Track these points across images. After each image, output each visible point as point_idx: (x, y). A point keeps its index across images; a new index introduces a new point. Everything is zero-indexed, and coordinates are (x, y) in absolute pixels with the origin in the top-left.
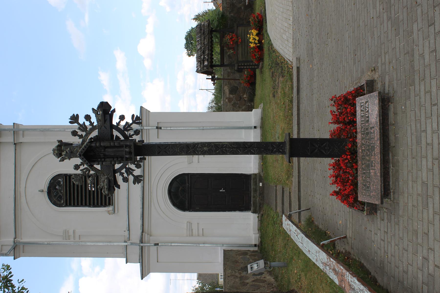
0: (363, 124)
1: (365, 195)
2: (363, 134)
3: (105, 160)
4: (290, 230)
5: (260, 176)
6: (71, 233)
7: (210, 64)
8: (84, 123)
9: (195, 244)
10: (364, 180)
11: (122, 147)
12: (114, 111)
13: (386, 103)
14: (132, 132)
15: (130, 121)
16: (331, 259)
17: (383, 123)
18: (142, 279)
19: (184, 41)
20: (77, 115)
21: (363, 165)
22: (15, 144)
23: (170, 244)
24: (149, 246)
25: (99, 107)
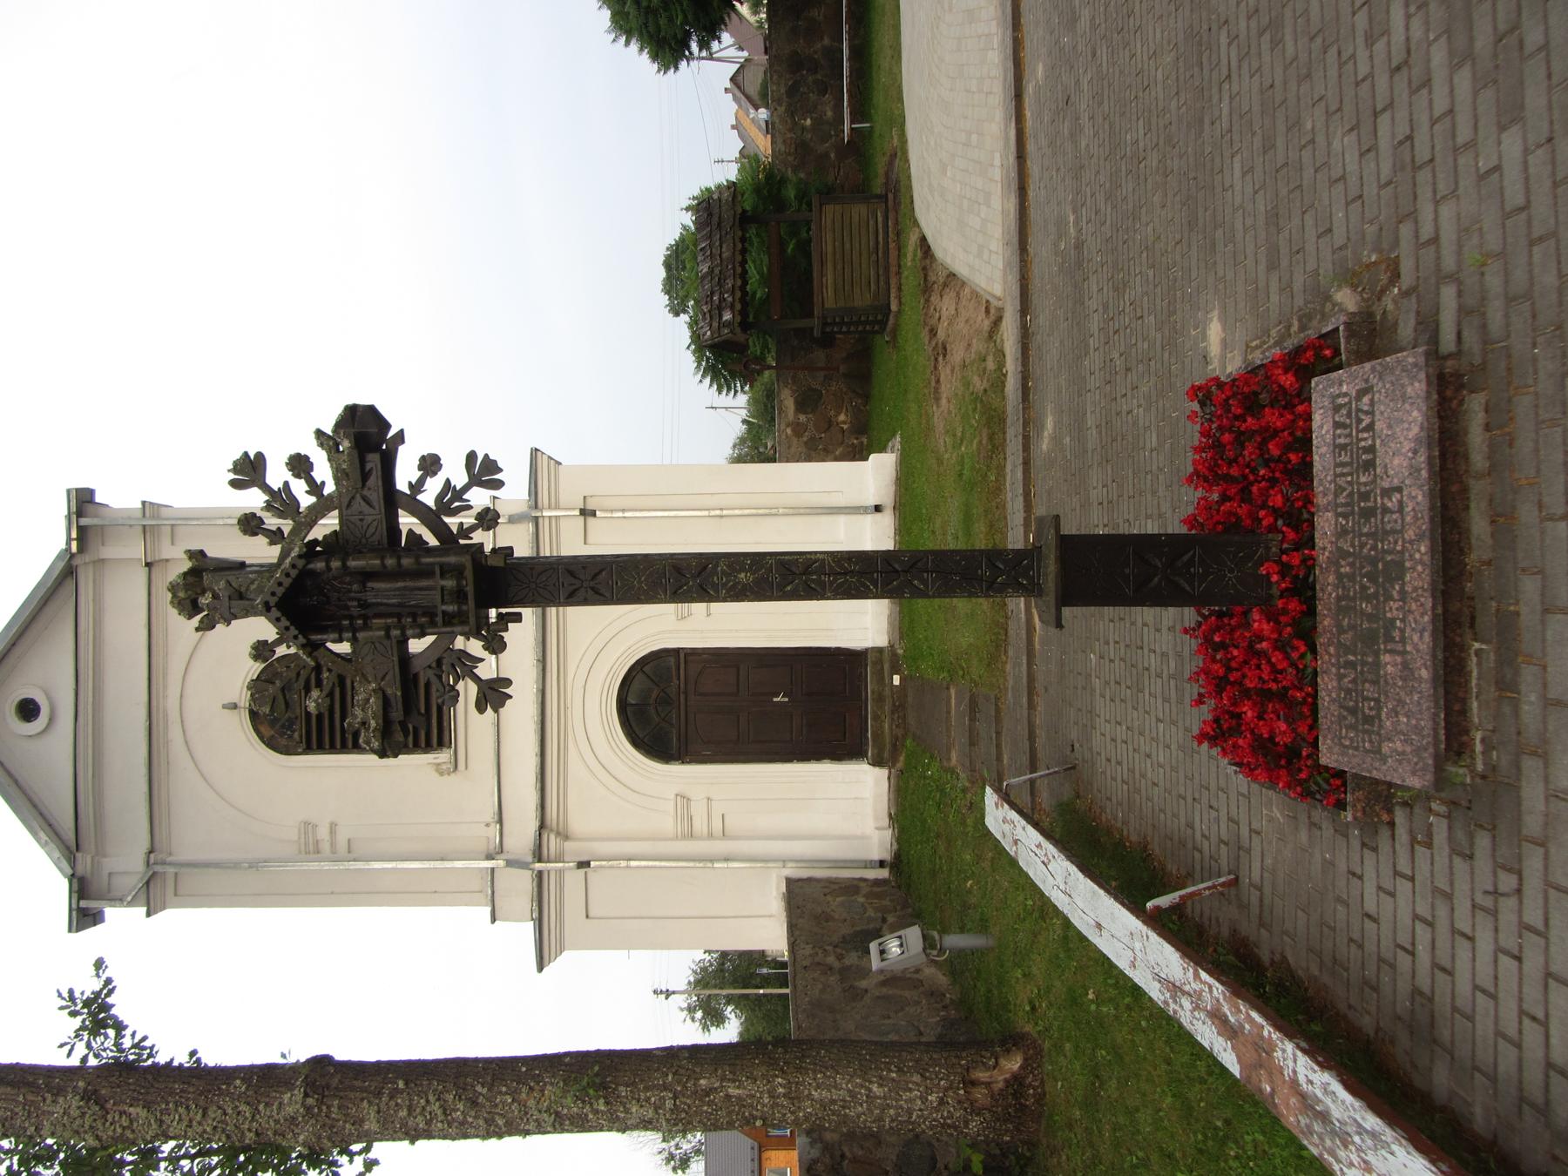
0: (1343, 475)
1: (1356, 749)
2: (1345, 516)
3: (365, 624)
4: (1016, 842)
5: (894, 654)
6: (323, 833)
7: (738, 319)
8: (286, 484)
9: (700, 860)
10: (1348, 691)
11: (426, 573)
12: (400, 437)
13: (1449, 393)
14: (468, 519)
15: (460, 479)
16: (1204, 975)
17: (1442, 468)
18: (540, 968)
19: (662, 274)
20: (260, 456)
21: (1341, 631)
22: (148, 565)
23: (623, 863)
24: (561, 872)
25: (339, 425)
